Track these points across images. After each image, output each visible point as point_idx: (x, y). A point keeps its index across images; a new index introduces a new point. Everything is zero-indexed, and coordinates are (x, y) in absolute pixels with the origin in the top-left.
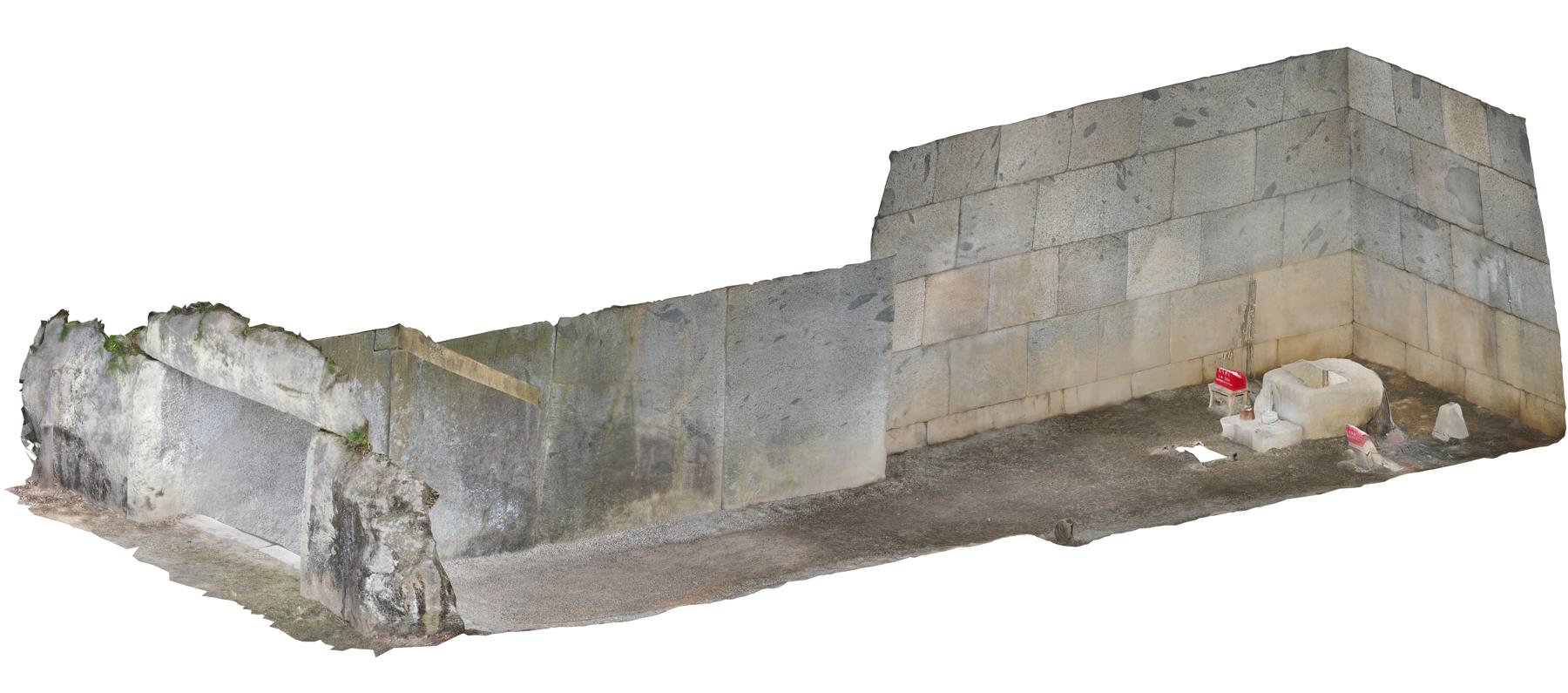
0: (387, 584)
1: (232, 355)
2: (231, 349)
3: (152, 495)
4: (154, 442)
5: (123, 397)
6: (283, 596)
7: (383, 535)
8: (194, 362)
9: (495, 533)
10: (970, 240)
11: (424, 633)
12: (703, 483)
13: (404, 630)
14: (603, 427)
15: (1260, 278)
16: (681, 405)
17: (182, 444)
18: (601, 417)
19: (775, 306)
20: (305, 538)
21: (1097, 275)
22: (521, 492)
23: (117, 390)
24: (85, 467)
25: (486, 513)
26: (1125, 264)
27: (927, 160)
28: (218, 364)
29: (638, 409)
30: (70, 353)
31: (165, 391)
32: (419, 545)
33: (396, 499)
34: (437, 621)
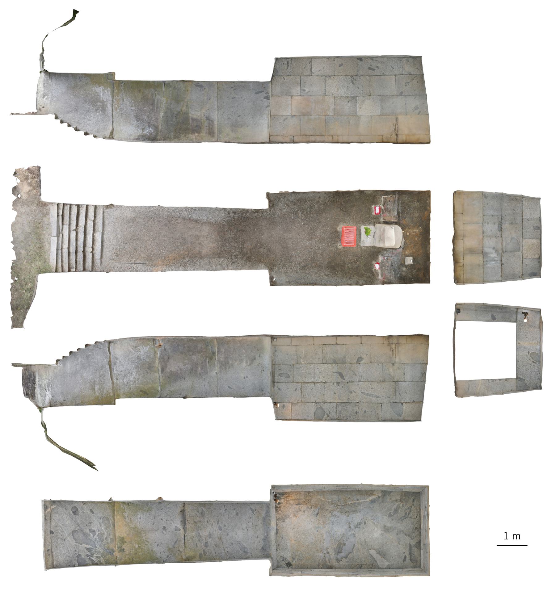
3: (41, 107)
4: (41, 93)
9: (146, 135)
10: (305, 89)
14: (179, 112)
15: (399, 117)
16: (204, 111)
19: (232, 89)
21: (347, 107)
22: (154, 125)
25: (143, 129)
26: (356, 105)
27: (288, 63)
29: (190, 110)
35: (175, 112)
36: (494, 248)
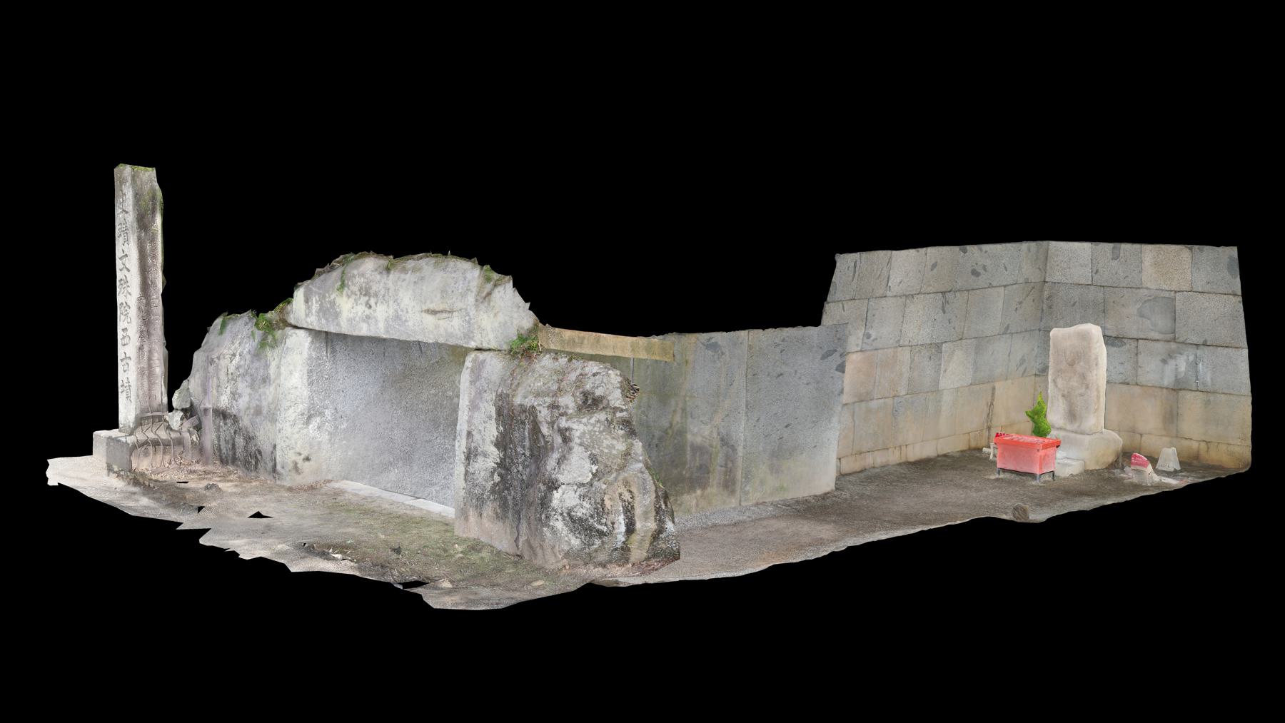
0: (582, 497)
1: (376, 295)
2: (374, 288)
3: (299, 460)
4: (301, 407)
5: (272, 371)
6: (435, 537)
7: (576, 434)
8: (337, 315)
11: (627, 561)
12: (729, 485)
13: (602, 557)
14: (666, 432)
15: (997, 385)
16: (718, 420)
17: (327, 412)
18: (665, 424)
20: (460, 469)
23: (267, 366)
24: (240, 441)
28: (361, 309)
29: (690, 420)
30: (227, 343)
31: (310, 358)
32: (621, 446)
33: (586, 395)
34: (647, 545)
35: (657, 433)
36: (1164, 361)
